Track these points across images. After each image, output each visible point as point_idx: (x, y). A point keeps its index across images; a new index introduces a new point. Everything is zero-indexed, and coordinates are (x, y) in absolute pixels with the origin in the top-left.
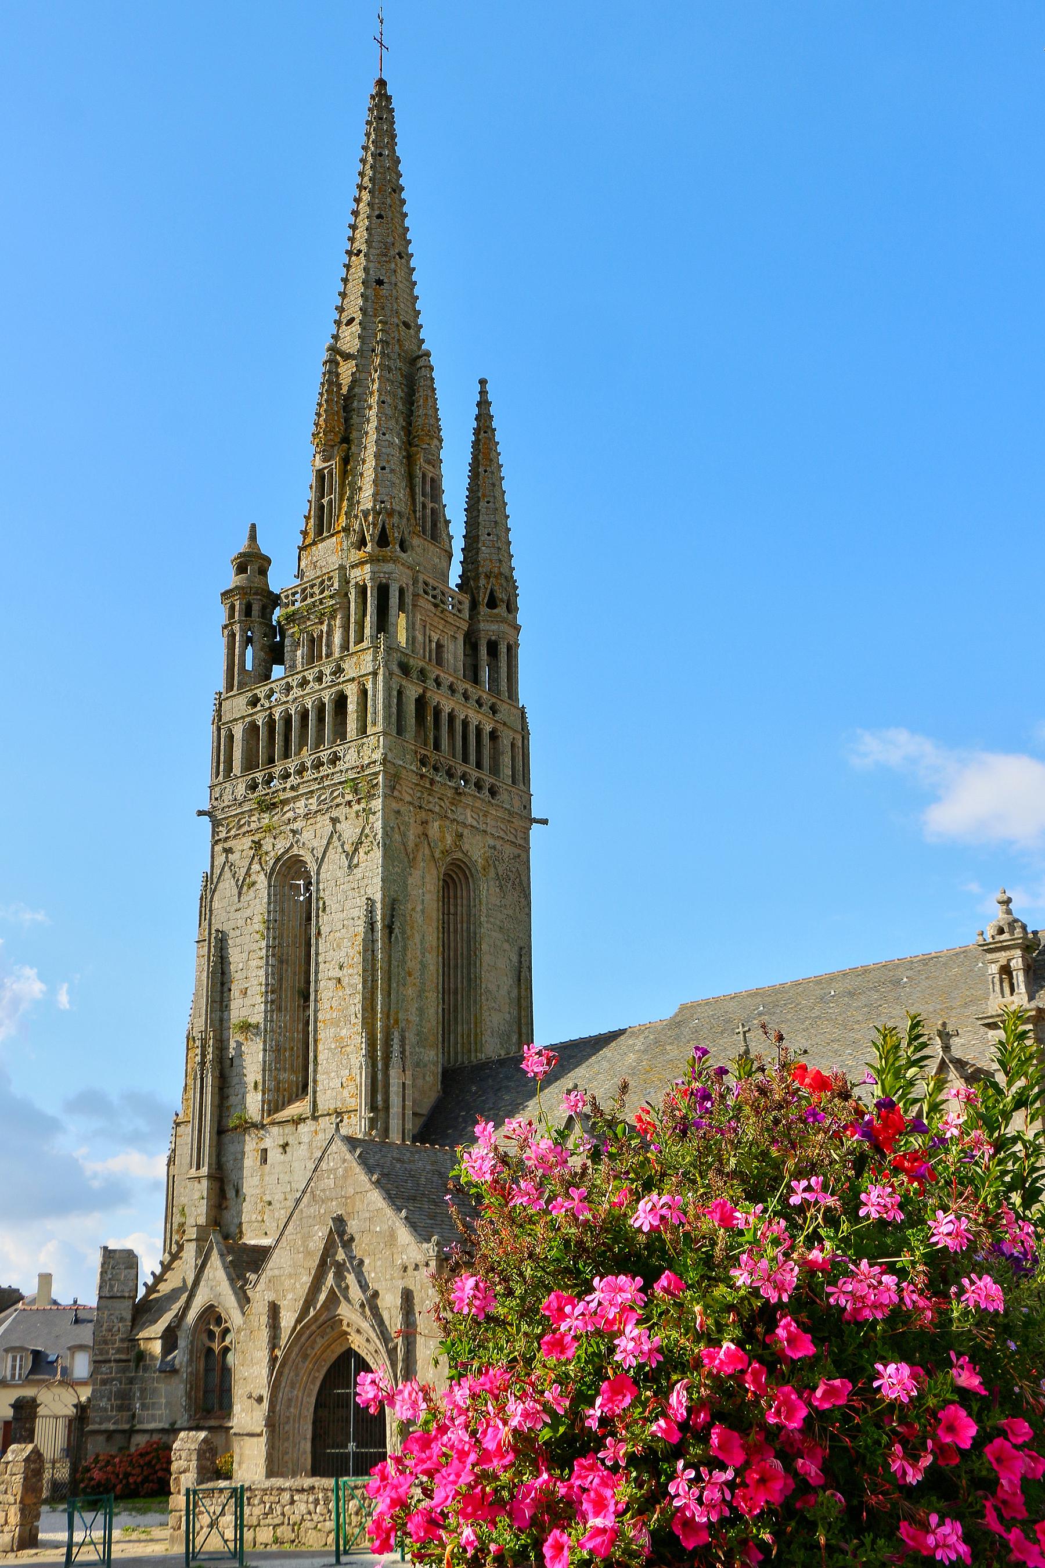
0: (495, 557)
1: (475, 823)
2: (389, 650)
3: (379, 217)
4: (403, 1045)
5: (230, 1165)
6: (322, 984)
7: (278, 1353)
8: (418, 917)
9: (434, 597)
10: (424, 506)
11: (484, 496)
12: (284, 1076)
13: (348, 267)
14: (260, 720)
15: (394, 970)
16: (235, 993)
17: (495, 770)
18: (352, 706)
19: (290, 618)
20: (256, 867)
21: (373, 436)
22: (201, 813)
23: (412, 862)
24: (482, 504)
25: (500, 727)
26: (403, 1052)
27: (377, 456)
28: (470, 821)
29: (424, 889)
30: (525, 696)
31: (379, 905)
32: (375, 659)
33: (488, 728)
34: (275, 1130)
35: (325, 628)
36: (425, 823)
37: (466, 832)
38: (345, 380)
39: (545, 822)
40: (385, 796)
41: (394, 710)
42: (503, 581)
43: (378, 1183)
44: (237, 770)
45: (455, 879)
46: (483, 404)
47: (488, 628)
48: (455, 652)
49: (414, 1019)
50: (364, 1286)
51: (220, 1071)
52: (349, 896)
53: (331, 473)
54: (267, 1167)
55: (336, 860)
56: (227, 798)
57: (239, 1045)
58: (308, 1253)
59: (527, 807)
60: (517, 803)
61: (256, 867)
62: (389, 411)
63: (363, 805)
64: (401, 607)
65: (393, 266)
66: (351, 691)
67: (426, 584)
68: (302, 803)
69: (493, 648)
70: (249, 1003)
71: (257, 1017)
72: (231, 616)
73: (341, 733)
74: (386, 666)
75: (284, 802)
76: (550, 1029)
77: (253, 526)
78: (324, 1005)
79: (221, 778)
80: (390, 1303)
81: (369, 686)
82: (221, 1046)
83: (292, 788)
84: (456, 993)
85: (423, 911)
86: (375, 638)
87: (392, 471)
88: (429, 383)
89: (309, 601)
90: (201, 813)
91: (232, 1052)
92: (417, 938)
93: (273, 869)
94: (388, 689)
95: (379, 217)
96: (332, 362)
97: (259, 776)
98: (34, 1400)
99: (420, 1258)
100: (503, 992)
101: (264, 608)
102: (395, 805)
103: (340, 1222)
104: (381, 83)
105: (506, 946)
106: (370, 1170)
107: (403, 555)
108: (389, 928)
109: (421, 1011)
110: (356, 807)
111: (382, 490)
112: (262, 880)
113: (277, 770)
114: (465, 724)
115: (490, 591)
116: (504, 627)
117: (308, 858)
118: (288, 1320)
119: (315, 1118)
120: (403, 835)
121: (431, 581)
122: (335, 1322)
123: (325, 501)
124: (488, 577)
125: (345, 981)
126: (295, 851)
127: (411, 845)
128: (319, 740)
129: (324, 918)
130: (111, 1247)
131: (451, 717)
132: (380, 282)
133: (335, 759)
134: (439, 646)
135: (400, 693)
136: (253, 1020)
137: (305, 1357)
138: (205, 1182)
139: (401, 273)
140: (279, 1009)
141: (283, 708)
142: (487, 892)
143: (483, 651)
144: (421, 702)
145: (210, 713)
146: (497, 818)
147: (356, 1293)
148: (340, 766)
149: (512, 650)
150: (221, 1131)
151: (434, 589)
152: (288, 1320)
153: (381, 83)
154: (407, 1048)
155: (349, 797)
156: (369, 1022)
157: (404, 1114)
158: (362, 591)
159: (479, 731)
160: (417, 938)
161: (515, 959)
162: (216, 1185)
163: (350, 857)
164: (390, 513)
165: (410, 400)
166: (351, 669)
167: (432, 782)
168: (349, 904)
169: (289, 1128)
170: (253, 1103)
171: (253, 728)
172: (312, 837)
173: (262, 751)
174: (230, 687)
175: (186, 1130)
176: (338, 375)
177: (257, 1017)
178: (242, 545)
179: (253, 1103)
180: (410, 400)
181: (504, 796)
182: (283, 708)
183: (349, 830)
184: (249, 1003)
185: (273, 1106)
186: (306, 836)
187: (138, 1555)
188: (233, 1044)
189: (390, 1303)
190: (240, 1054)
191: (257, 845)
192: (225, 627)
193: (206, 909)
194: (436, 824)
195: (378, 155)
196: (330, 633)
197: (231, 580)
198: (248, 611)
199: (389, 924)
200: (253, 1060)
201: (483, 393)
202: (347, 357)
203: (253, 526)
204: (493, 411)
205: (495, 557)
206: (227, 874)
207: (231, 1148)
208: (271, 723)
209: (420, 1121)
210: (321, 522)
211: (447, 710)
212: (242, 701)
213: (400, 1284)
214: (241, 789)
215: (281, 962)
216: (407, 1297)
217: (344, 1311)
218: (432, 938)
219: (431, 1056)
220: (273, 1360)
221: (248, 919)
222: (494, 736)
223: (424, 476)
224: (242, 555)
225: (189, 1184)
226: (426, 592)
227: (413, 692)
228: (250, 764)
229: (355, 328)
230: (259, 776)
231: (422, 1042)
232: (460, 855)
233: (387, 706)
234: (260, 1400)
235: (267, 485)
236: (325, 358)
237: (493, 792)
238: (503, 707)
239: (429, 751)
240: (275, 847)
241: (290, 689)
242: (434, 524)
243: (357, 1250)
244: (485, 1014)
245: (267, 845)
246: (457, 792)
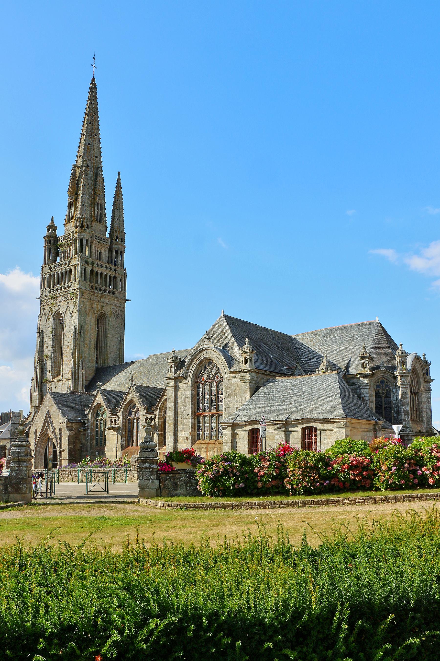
0: (118, 226)
1: (108, 302)
2: (82, 257)
3: (90, 123)
4: (83, 363)
5: (44, 391)
6: (64, 346)
7: (37, 440)
8: (89, 329)
9: (99, 240)
10: (98, 213)
11: (117, 208)
13: (81, 138)
15: (81, 344)
16: (45, 347)
18: (73, 273)
19: (61, 245)
20: (50, 314)
21: (81, 195)
22: (37, 298)
23: (88, 315)
24: (116, 210)
25: (117, 275)
26: (82, 365)
27: (82, 201)
28: (106, 302)
29: (91, 322)
30: (125, 266)
32: (78, 260)
33: (113, 276)
34: (54, 383)
36: (92, 304)
37: (105, 305)
38: (77, 175)
39: (130, 300)
40: (80, 298)
41: (83, 274)
42: (121, 233)
43: (56, 404)
44: (46, 287)
45: (101, 319)
46: (119, 179)
49: (87, 356)
50: (52, 427)
51: (41, 368)
52: (71, 323)
55: (68, 314)
56: (44, 294)
57: (46, 360)
58: (43, 419)
59: (125, 296)
60: (121, 295)
61: (50, 314)
62: (86, 188)
63: (75, 300)
64: (87, 244)
65: (93, 139)
66: (73, 268)
67: (96, 236)
68: (61, 298)
69: (116, 252)
70: (48, 351)
71: (50, 354)
72: (46, 244)
74: (81, 262)
75: (57, 297)
77: (53, 217)
78: (65, 352)
80: (57, 431)
81: (77, 268)
82: (42, 360)
83: (59, 294)
84: (101, 348)
85: (91, 328)
87: (86, 206)
88: (101, 176)
89: (65, 241)
90: (37, 298)
91: (44, 363)
92: (89, 335)
93: (54, 315)
94: (81, 269)
95: (90, 123)
96: (74, 170)
97: (51, 289)
98: (5, 446)
99: (63, 421)
100: (115, 347)
101: (54, 241)
102: (83, 300)
103: (48, 412)
104: (93, 80)
105: (116, 335)
106: (55, 400)
107: (88, 230)
108: (80, 333)
109: (89, 354)
110: (73, 300)
111: (83, 211)
112: (51, 317)
114: (106, 275)
115: (118, 235)
116: (120, 246)
117: (62, 313)
118: (38, 433)
119: (62, 381)
120: (85, 308)
121: (98, 235)
122: (48, 434)
124: (116, 232)
125: (69, 346)
126: (59, 311)
127: (87, 310)
128: (65, 282)
129: (65, 329)
131: (101, 274)
132: (89, 144)
133: (69, 287)
134: (100, 253)
135: (85, 269)
136: (49, 355)
137: (42, 442)
138: (37, 395)
139: (96, 141)
140: (55, 352)
141: (57, 271)
142: (111, 321)
143: (114, 253)
144: (92, 271)
146: (115, 300)
147: (51, 428)
148: (70, 289)
149: (122, 253)
150: (42, 383)
151: (99, 237)
152: (38, 433)
153: (93, 80)
154: (84, 364)
155: (72, 297)
157: (82, 381)
159: (110, 277)
160: (89, 335)
161: (119, 338)
162: (40, 396)
163: (71, 313)
164: (84, 219)
165: (95, 180)
166: (72, 263)
167: (94, 293)
168: (71, 326)
169: (57, 383)
170: (49, 376)
171: (50, 276)
172: (63, 307)
173: (52, 282)
174: (45, 264)
175: (34, 381)
176: (75, 174)
177: (50, 354)
178: (49, 223)
179: (49, 376)
180: (95, 180)
181: (117, 294)
182: (57, 271)
183: (71, 306)
184: (48, 351)
185: (54, 377)
186: (62, 307)
187: (319, 496)
188: (44, 360)
189: (57, 431)
190: (46, 363)
191: (51, 308)
192: (44, 247)
193: (39, 325)
194: (96, 304)
195: (91, 103)
196: (70, 250)
197: (46, 233)
198: (50, 242)
199: (80, 331)
201: (119, 176)
202: (79, 167)
203: (53, 217)
205: (118, 226)
206: (44, 315)
207: (44, 387)
208: (54, 275)
209: (88, 382)
210: (69, 217)
211: (100, 272)
212: (48, 268)
213: (60, 427)
214: (47, 293)
215: (56, 340)
216: (61, 430)
217: (49, 432)
218: (93, 335)
220: (36, 442)
221: (48, 327)
222: (115, 277)
223: (98, 204)
224: (49, 226)
226: (96, 239)
227: (89, 268)
228: (49, 286)
229: (81, 159)
230: (51, 289)
231: (89, 361)
232: (103, 312)
233: (81, 273)
235: (56, 207)
236: (72, 169)
237: (114, 293)
238: (118, 269)
239: (94, 284)
240: (55, 309)
242: (101, 217)
243: (52, 418)
244: (109, 353)
245: (53, 309)
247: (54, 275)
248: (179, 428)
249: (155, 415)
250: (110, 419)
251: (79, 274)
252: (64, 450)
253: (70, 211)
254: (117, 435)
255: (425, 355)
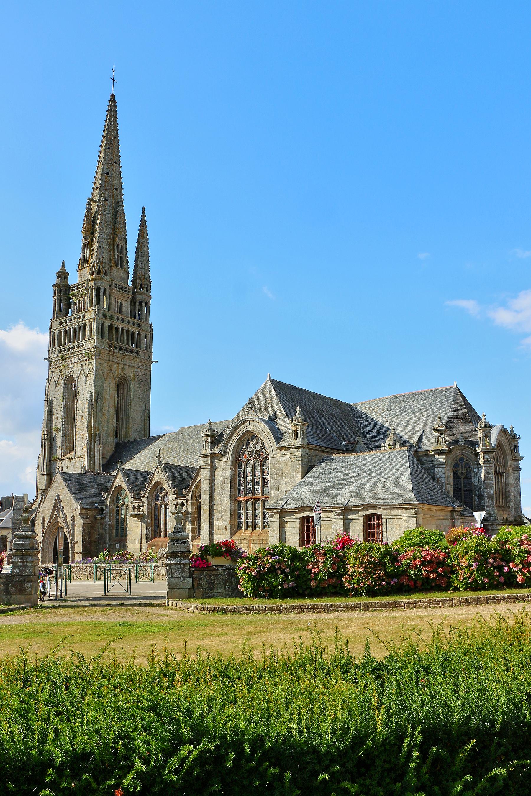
0: (143, 272)
1: (130, 364)
2: (99, 310)
3: (109, 148)
4: (100, 438)
5: (53, 471)
6: (78, 417)
7: (44, 530)
8: (108, 397)
9: (119, 288)
10: (118, 256)
11: (141, 250)
13: (97, 167)
15: (98, 414)
16: (54, 418)
18: (88, 329)
19: (73, 295)
20: (61, 378)
21: (98, 235)
22: (45, 359)
23: (106, 379)
24: (140, 253)
25: (141, 331)
26: (100, 440)
27: (98, 243)
28: (128, 363)
29: (110, 388)
30: (151, 320)
32: (94, 313)
33: (136, 332)
34: (65, 461)
36: (111, 366)
37: (127, 367)
38: (93, 211)
39: (157, 362)
40: (96, 359)
41: (100, 330)
42: (146, 281)
43: (68, 486)
44: (56, 346)
45: (122, 384)
46: (143, 216)
49: (105, 428)
50: (63, 514)
51: (50, 443)
52: (86, 389)
55: (82, 378)
56: (53, 355)
57: (55, 434)
58: (52, 504)
59: (151, 357)
60: (146, 355)
61: (61, 378)
62: (103, 226)
63: (90, 361)
64: (105, 294)
65: (112, 167)
66: (88, 323)
67: (116, 284)
68: (73, 359)
69: (141, 303)
70: (58, 422)
71: (60, 426)
72: (55, 294)
74: (98, 315)
75: (69, 358)
77: (64, 261)
78: (78, 424)
80: (69, 518)
81: (93, 322)
82: (50, 434)
83: (71, 354)
84: (122, 419)
85: (109, 395)
87: (103, 248)
88: (121, 212)
89: (79, 290)
90: (45, 359)
91: (54, 437)
92: (107, 403)
93: (65, 379)
94: (98, 323)
95: (109, 148)
96: (89, 205)
97: (62, 348)
98: (6, 537)
99: (76, 507)
100: (139, 418)
101: (66, 290)
102: (100, 361)
103: (58, 496)
104: (113, 96)
105: (140, 403)
106: (66, 482)
107: (106, 277)
108: (96, 401)
109: (108, 426)
110: (88, 362)
111: (100, 255)
112: (62, 382)
114: (128, 331)
115: (142, 283)
116: (145, 297)
117: (75, 376)
118: (46, 522)
119: (75, 458)
120: (103, 371)
121: (118, 284)
122: (57, 523)
124: (140, 279)
125: (84, 417)
126: (71, 374)
127: (105, 373)
128: (79, 340)
129: (79, 396)
131: (122, 330)
132: (107, 174)
133: (83, 346)
134: (121, 304)
135: (103, 324)
136: (59, 427)
137: (51, 532)
138: (45, 476)
139: (115, 170)
140: (67, 424)
141: (68, 327)
142: (134, 386)
143: (137, 305)
144: (111, 327)
146: (139, 362)
147: (61, 515)
148: (84, 348)
149: (148, 304)
150: (50, 461)
151: (119, 286)
152: (46, 522)
153: (113, 96)
154: (101, 438)
155: (86, 358)
157: (99, 458)
159: (133, 333)
160: (107, 403)
161: (144, 407)
162: (49, 477)
163: (86, 377)
164: (102, 263)
165: (115, 217)
166: (87, 317)
167: (114, 352)
168: (85, 393)
169: (69, 461)
170: (59, 452)
171: (60, 332)
172: (76, 370)
173: (63, 340)
174: (54, 318)
175: (41, 459)
176: (91, 209)
177: (60, 426)
178: (59, 269)
179: (59, 452)
180: (115, 217)
181: (141, 354)
182: (68, 327)
183: (86, 369)
184: (58, 422)
185: (65, 454)
186: (74, 369)
187: (385, 598)
188: (54, 434)
189: (69, 518)
190: (56, 437)
191: (61, 371)
192: (53, 297)
193: (47, 392)
194: (115, 366)
195: (110, 124)
196: (84, 301)
197: (55, 281)
198: (60, 292)
199: (97, 399)
201: (143, 212)
202: (95, 202)
203: (64, 261)
205: (143, 272)
206: (53, 380)
207: (53, 466)
208: (65, 331)
209: (106, 460)
210: (84, 261)
211: (121, 328)
212: (57, 323)
213: (72, 514)
214: (57, 353)
215: (68, 409)
216: (73, 517)
217: (59, 520)
218: (113, 403)
220: (43, 532)
221: (58, 394)
222: (139, 334)
223: (118, 245)
224: (59, 272)
226: (116, 287)
227: (107, 323)
228: (60, 345)
229: (98, 191)
230: (62, 348)
231: (108, 435)
232: (124, 375)
233: (98, 329)
235: (67, 249)
236: (87, 203)
237: (137, 353)
238: (143, 325)
239: (114, 342)
240: (66, 372)
242: (121, 262)
243: (63, 504)
244: (131, 426)
245: (64, 372)
247: (65, 331)
248: (216, 515)
249: (187, 500)
250: (133, 505)
251: (95, 329)
252: (77, 542)
253: (85, 254)
254: (141, 524)
255: (513, 428)
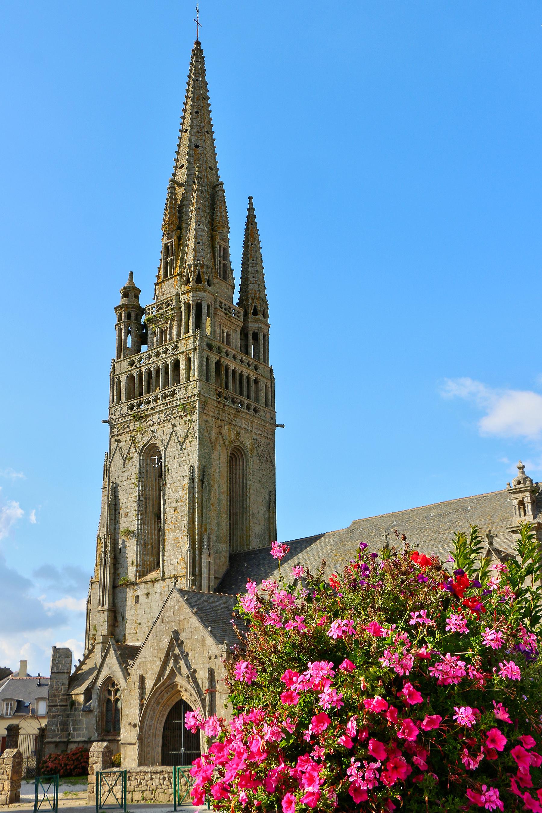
0: (257, 289)
1: (246, 427)
2: (202, 337)
3: (197, 112)
4: (209, 542)
5: (119, 604)
6: (167, 510)
7: (144, 701)
8: (217, 476)
9: (225, 309)
10: (220, 263)
11: (251, 257)
12: (147, 558)
13: (180, 138)
14: (135, 373)
15: (205, 503)
16: (122, 515)
17: (257, 399)
18: (182, 366)
19: (151, 320)
20: (133, 449)
21: (193, 226)
22: (104, 422)
23: (214, 447)
24: (250, 261)
25: (259, 377)
26: (209, 546)
27: (196, 236)
28: (244, 426)
29: (220, 461)
30: (272, 361)
31: (196, 469)
32: (194, 342)
33: (253, 378)
34: (142, 586)
35: (168, 325)
36: (220, 427)
37: (242, 431)
38: (179, 197)
39: (282, 426)
40: (200, 413)
41: (204, 368)
42: (261, 301)
43: (196, 614)
44: (123, 399)
45: (236, 456)
46: (251, 209)
47: (253, 326)
48: (236, 338)
49: (215, 528)
50: (189, 667)
51: (114, 555)
52: (181, 465)
53: (171, 245)
54: (139, 605)
55: (174, 446)
56: (118, 414)
57: (124, 542)
58: (160, 650)
59: (273, 418)
60: (268, 416)
61: (133, 449)
62: (202, 213)
63: (188, 417)
64: (208, 315)
65: (204, 138)
66: (182, 358)
67: (221, 303)
68: (157, 416)
69: (256, 336)
70: (129, 520)
71: (133, 527)
72: (120, 319)
73: (177, 380)
74: (200, 345)
75: (147, 416)
76: (285, 533)
77: (131, 273)
78: (168, 521)
79: (114, 403)
80: (202, 676)
81: (191, 356)
82: (115, 542)
83: (152, 409)
84: (236, 515)
85: (219, 472)
86: (194, 331)
87: (203, 244)
88: (222, 198)
89: (160, 311)
90: (104, 422)
91: (120, 546)
92: (216, 486)
93: (141, 451)
94: (201, 357)
95: (197, 112)
96: (172, 188)
97: (134, 402)
98: (18, 726)
99: (218, 652)
100: (261, 514)
101: (137, 315)
102: (205, 418)
103: (176, 633)
104: (198, 43)
105: (263, 491)
106: (192, 607)
107: (209, 288)
108: (202, 481)
109: (218, 524)
110: (185, 419)
111: (198, 254)
112: (136, 456)
113: (144, 399)
114: (241, 375)
115: (254, 307)
116: (261, 325)
117: (160, 445)
118: (149, 684)
119: (163, 580)
120: (209, 433)
121: (223, 301)
122: (174, 686)
123: (169, 260)
124: (253, 299)
125: (179, 509)
126: (153, 441)
127: (213, 438)
128: (166, 384)
129: (168, 476)
130: (58, 646)
131: (234, 372)
132: (197, 146)
133: (174, 394)
134: (228, 335)
135: (207, 359)
136: (131, 529)
137: (158, 703)
138: (106, 613)
139: (208, 142)
140: (145, 523)
141: (147, 367)
142: (253, 462)
143: (251, 337)
144: (218, 364)
145: (109, 370)
146: (258, 424)
147: (184, 670)
148: (177, 397)
149: (265, 337)
150: (114, 586)
151: (225, 305)
152: (149, 684)
153: (198, 43)
154: (211, 543)
155: (181, 413)
156: (191, 530)
157: (209, 578)
158: (188, 306)
159: (248, 379)
160: (216, 486)
161: (267, 497)
162: (112, 614)
163: (181, 444)
164: (203, 266)
165: (213, 207)
166: (182, 347)
167: (224, 405)
168: (181, 469)
169: (150, 585)
170: (131, 572)
171: (131, 378)
172: (162, 434)
173: (136, 390)
174: (119, 356)
175: (96, 586)
176: (175, 194)
177: (133, 527)
178: (125, 283)
179: (131, 572)
180: (213, 207)
181: (261, 413)
182: (147, 367)
183: (181, 430)
184: (129, 520)
185: (141, 574)
186: (159, 433)
187: (71, 806)
188: (121, 541)
189: (202, 676)
190: (124, 547)
191: (134, 438)
192: (117, 325)
193: (107, 472)
194: (226, 427)
195: (196, 81)
196: (171, 328)
197: (120, 301)
198: (128, 317)
199: (202, 479)
200: (131, 550)
201: (251, 204)
202: (180, 185)
203: (131, 273)
204: (255, 213)
205: (257, 289)
206: (118, 453)
207: (120, 595)
208: (140, 375)
209: (218, 581)
210: (167, 271)
211: (232, 368)
212: (125, 363)
213: (208, 666)
214: (125, 409)
215: (146, 499)
216: (211, 672)
217: (179, 680)
218: (224, 487)
219: (224, 547)
220: (142, 705)
221: (129, 477)
222: (256, 381)
223: (220, 247)
224: (125, 288)
225: (98, 614)
226: (221, 307)
227: (214, 359)
228: (130, 396)
229: (184, 170)
230: (134, 402)
231: (219, 540)
232: (239, 444)
233: (201, 366)
234: (135, 726)
235: (138, 251)
236: (169, 186)
237: (256, 411)
238: (261, 367)
239: (222, 390)
240: (143, 439)
241: (150, 357)
242: (225, 272)
243: (185, 648)
244: (252, 526)
245: (138, 438)
246: (237, 411)
